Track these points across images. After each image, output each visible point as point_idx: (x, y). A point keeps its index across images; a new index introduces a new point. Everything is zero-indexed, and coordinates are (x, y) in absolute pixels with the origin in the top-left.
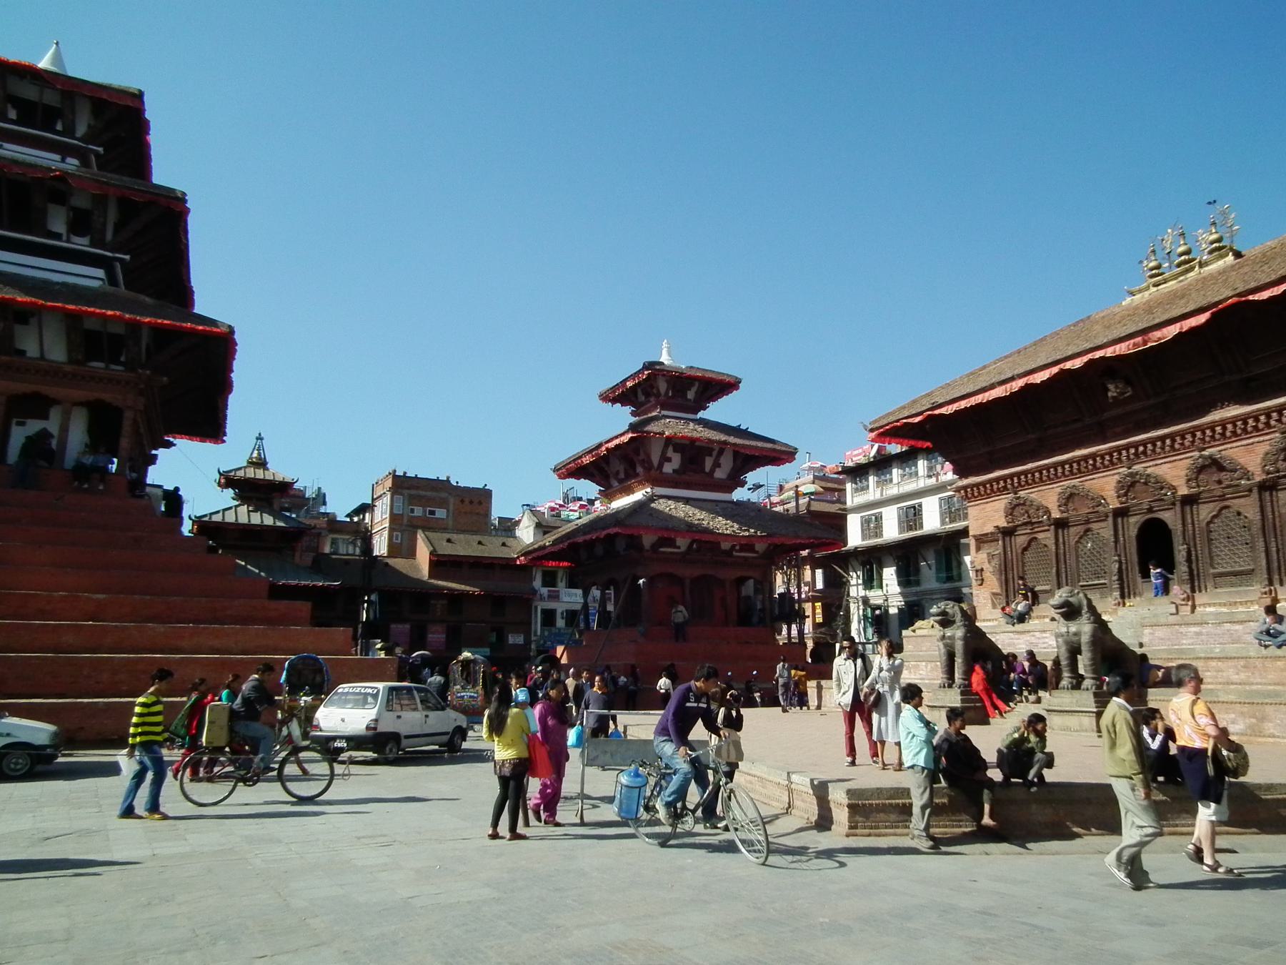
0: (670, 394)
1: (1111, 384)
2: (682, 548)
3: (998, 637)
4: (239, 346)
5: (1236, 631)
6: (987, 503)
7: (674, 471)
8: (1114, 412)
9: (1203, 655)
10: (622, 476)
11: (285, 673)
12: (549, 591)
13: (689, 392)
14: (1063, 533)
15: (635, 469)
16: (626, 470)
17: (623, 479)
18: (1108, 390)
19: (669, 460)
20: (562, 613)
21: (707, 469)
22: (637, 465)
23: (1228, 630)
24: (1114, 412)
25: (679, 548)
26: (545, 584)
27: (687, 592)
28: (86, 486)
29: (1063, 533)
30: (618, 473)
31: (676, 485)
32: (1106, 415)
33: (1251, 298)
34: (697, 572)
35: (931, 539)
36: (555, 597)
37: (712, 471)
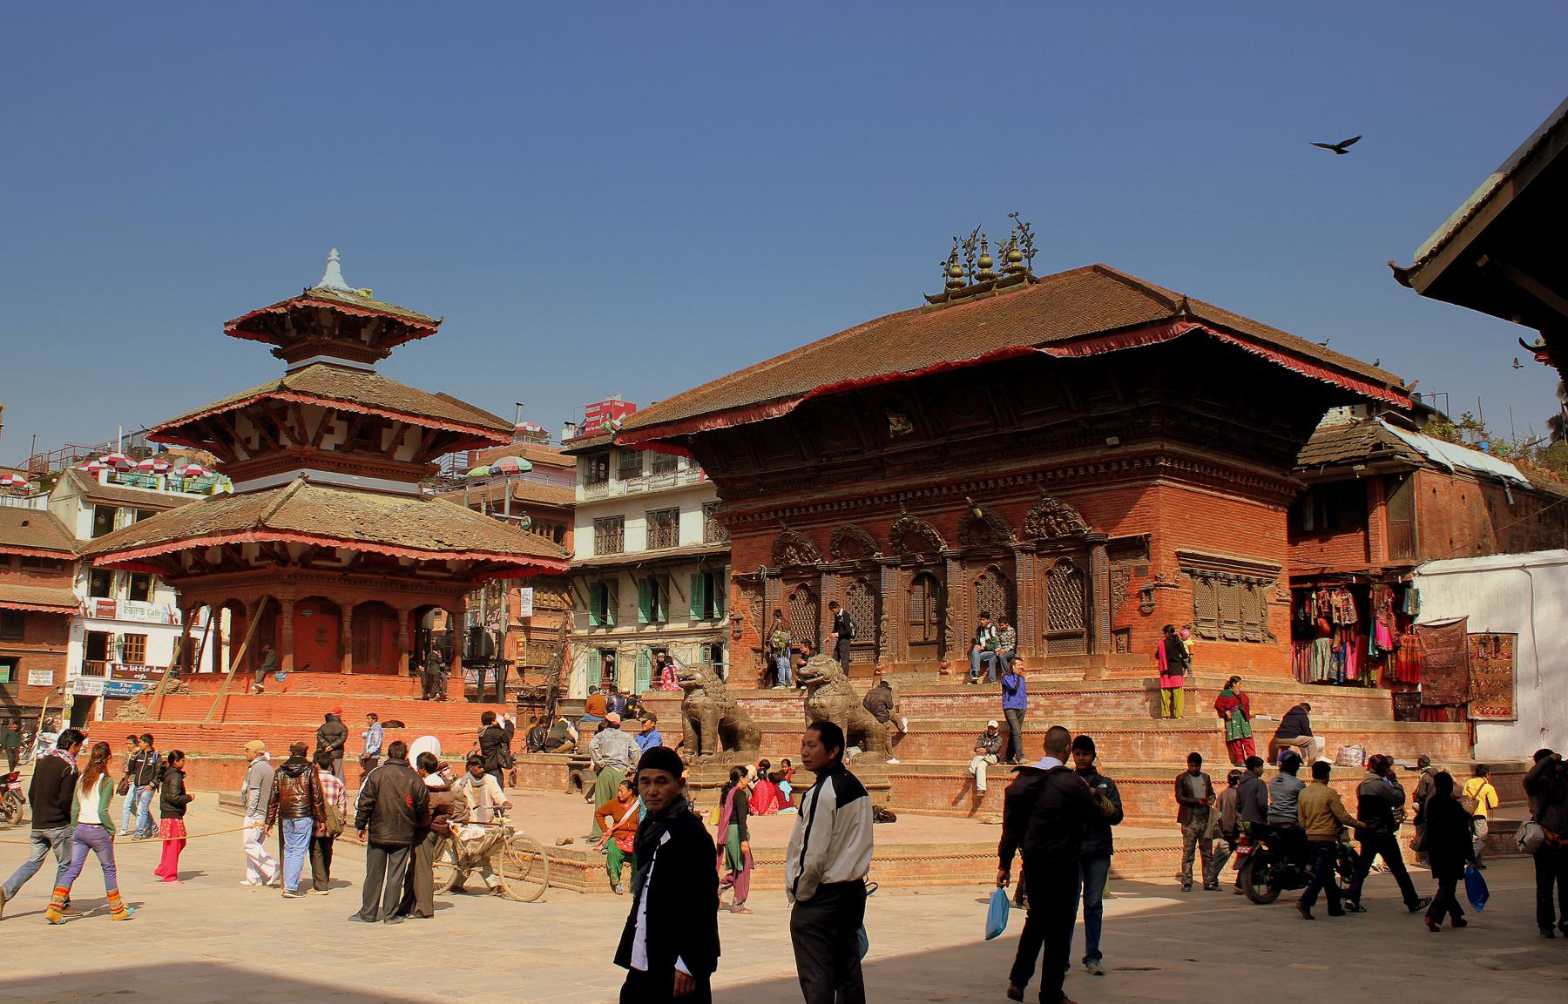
0: (337, 333)
1: (893, 416)
2: (343, 561)
3: (752, 704)
4: (1429, 452)
5: (983, 704)
6: (754, 537)
7: (337, 447)
8: (899, 448)
9: (946, 730)
10: (255, 445)
11: (403, 889)
12: (99, 603)
13: (363, 330)
14: (1322, 675)
15: (277, 439)
16: (262, 439)
17: (257, 452)
18: (889, 423)
19: (331, 431)
20: (766, 761)
21: (384, 448)
22: (282, 432)
23: (976, 703)
24: (899, 448)
25: (339, 560)
26: (94, 592)
27: (347, 625)
28: (362, 560)
29: (1322, 675)
30: (248, 440)
31: (338, 467)
32: (887, 451)
33: (1043, 350)
34: (362, 598)
35: (630, 568)
36: (108, 614)
37: (392, 449)
